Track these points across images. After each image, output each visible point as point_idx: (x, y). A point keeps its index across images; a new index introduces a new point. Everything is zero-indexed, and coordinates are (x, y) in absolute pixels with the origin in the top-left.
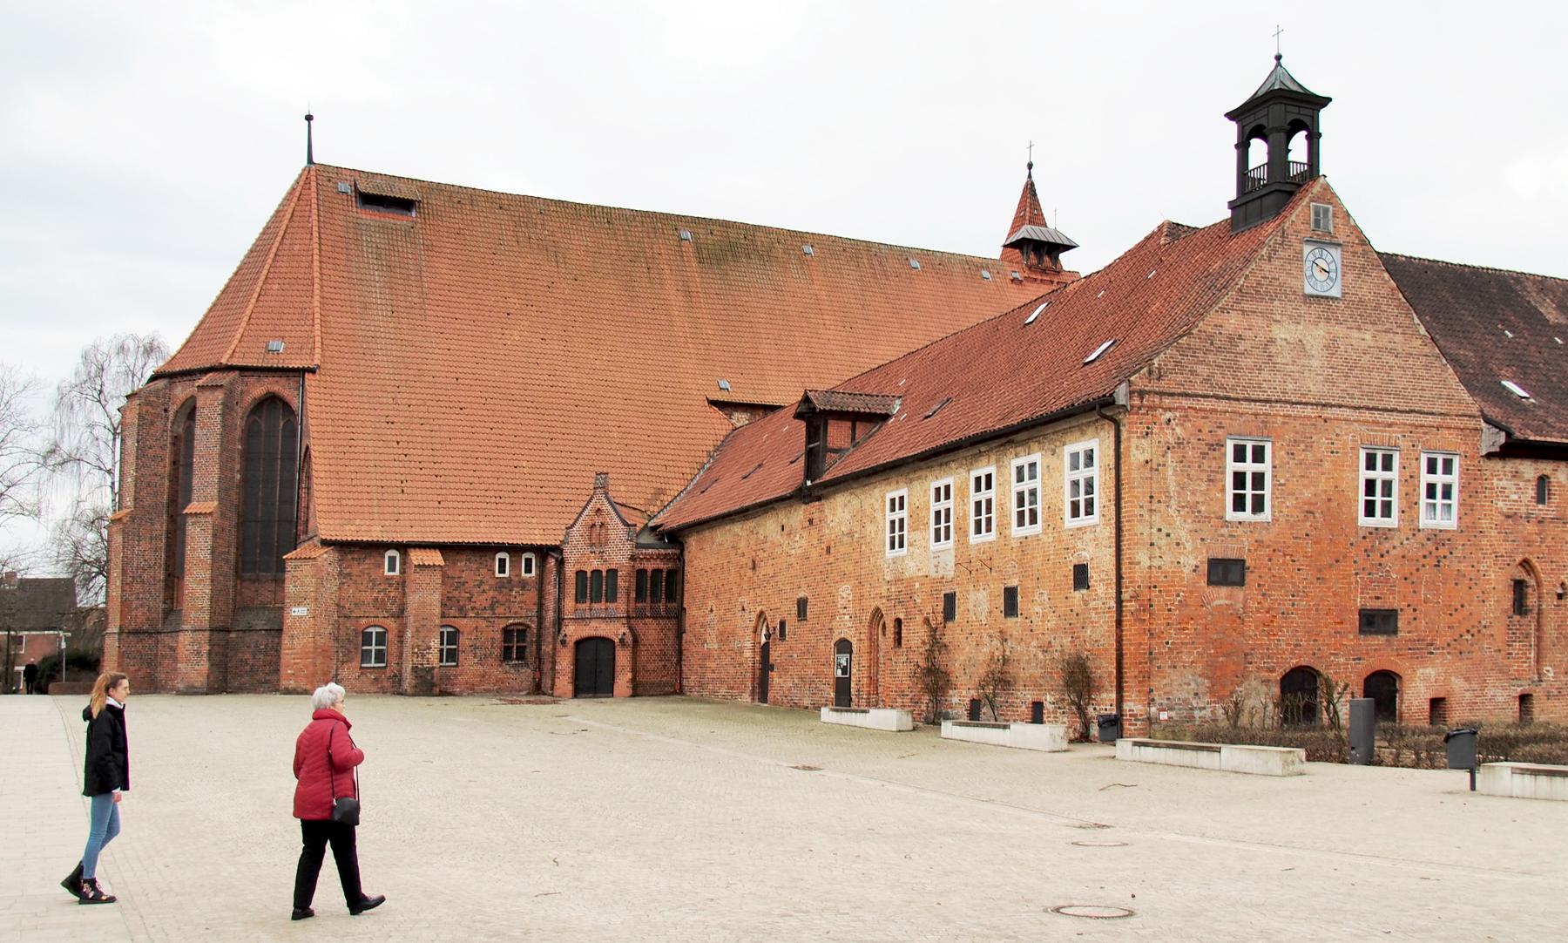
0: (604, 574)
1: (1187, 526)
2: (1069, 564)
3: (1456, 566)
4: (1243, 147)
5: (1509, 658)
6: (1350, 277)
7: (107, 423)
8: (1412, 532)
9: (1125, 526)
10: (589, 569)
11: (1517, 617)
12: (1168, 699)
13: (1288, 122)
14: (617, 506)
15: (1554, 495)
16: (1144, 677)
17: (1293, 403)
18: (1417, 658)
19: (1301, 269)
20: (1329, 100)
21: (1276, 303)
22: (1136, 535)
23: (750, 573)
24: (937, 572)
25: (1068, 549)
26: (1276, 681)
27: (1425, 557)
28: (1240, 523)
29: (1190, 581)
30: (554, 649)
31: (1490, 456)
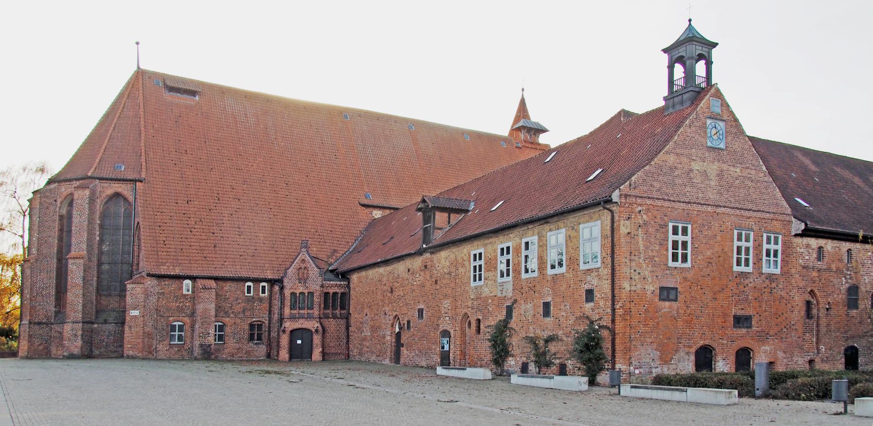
0: (306, 294)
1: (649, 269)
2: (582, 289)
3: (780, 293)
4: (671, 68)
5: (803, 341)
6: (729, 138)
7: (19, 208)
8: (759, 275)
9: (617, 268)
10: (298, 292)
11: (807, 320)
12: (639, 362)
13: (697, 54)
14: (313, 259)
15: (825, 257)
16: (627, 350)
17: (702, 204)
18: (761, 341)
19: (706, 133)
20: (717, 44)
21: (693, 150)
22: (623, 273)
23: (389, 295)
24: (502, 294)
25: (582, 281)
26: (693, 353)
27: (765, 288)
28: (675, 268)
29: (651, 299)
30: (278, 334)
31: (796, 235)
